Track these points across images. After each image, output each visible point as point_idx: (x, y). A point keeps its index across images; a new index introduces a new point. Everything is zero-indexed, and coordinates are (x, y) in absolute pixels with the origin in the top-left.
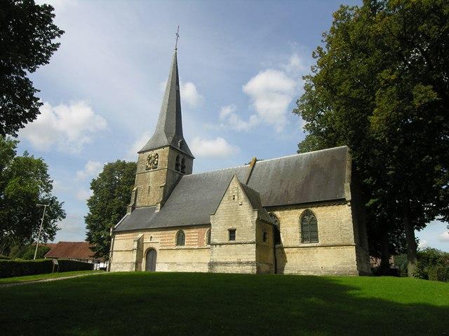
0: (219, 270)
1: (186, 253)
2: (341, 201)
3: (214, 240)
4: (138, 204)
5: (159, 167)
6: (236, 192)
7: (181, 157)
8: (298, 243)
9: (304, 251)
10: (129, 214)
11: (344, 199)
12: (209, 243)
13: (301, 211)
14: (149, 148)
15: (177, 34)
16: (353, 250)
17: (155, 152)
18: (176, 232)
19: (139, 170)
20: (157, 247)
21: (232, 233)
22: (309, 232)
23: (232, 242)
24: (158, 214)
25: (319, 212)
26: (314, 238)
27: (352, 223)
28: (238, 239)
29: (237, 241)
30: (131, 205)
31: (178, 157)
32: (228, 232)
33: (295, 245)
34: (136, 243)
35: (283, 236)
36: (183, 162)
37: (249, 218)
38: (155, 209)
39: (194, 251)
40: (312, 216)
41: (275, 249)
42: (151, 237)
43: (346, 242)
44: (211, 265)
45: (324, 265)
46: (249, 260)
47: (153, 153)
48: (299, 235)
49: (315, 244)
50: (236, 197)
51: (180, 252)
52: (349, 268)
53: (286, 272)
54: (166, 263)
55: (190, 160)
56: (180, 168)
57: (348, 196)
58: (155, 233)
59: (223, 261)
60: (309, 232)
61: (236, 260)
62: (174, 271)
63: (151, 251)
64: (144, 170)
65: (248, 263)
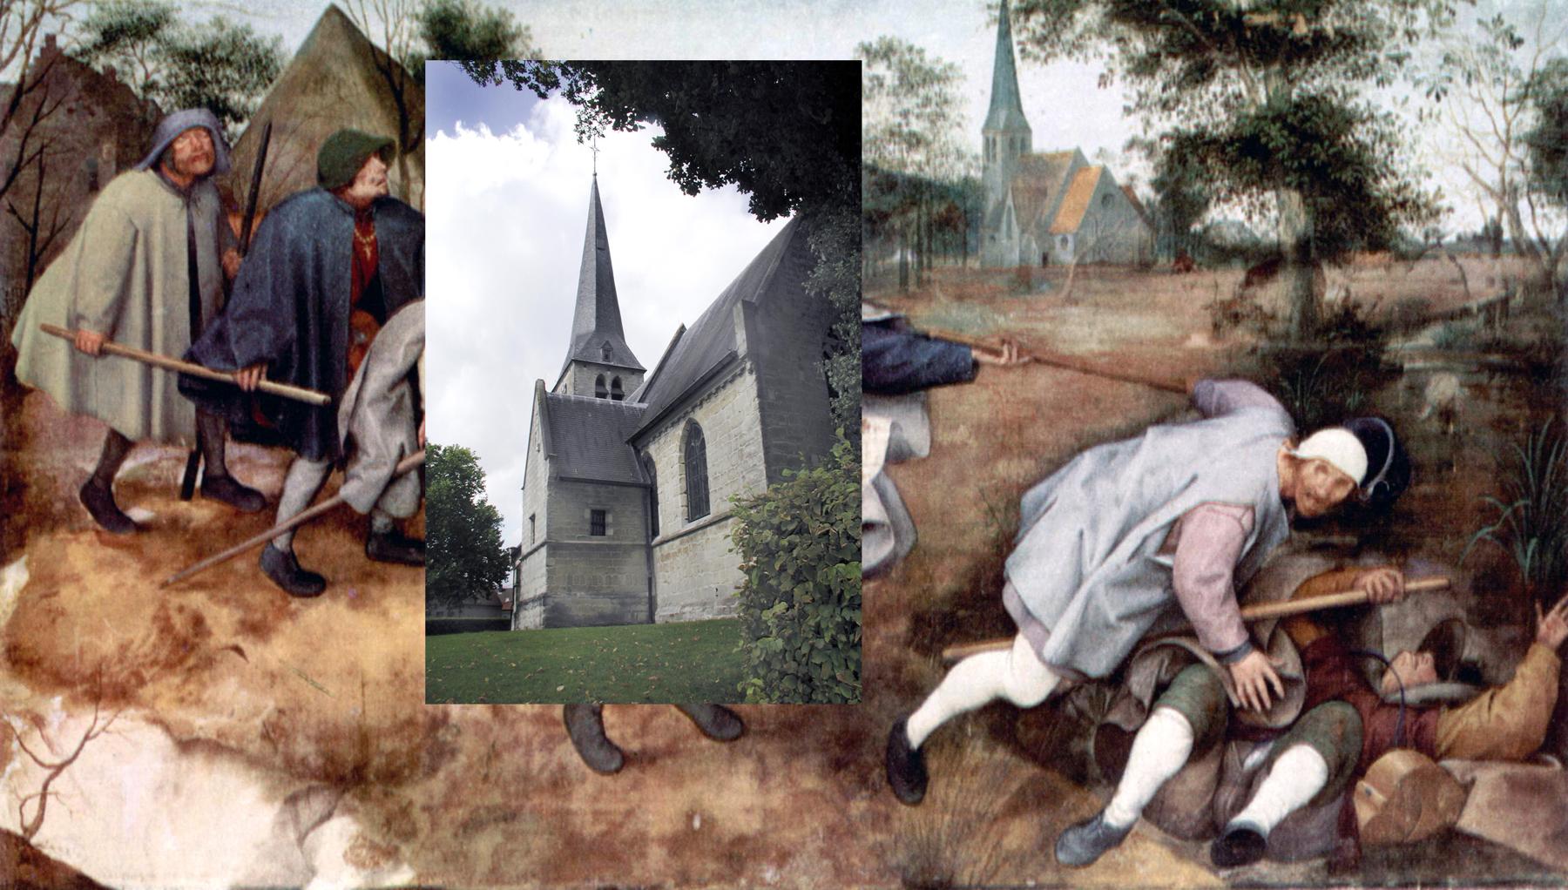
11: (733, 357)
31: (600, 382)
55: (635, 377)
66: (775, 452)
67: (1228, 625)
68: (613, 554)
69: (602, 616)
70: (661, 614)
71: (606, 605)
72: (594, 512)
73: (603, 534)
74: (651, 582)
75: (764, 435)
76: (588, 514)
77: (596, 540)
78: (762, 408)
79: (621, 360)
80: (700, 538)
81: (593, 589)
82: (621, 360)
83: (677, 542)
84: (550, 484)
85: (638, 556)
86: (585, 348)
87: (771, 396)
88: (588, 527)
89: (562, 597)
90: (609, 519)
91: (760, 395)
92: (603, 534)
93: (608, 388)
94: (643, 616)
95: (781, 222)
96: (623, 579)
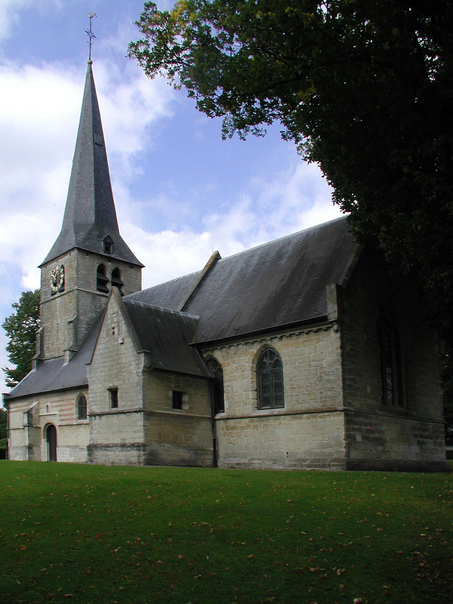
1: (295, 423)
2: (318, 323)
3: (92, 407)
4: (47, 355)
5: (67, 288)
6: (115, 320)
7: (110, 267)
8: (249, 409)
9: (260, 424)
10: (34, 371)
11: (324, 319)
12: (82, 413)
13: (255, 349)
14: (52, 258)
15: (89, 33)
16: (340, 419)
19: (43, 299)
20: (56, 422)
21: (114, 392)
22: (269, 388)
23: (115, 410)
24: (67, 366)
25: (287, 348)
26: (279, 401)
27: (340, 367)
28: (122, 404)
29: (119, 409)
30: (36, 356)
31: (101, 270)
32: (107, 394)
33: (246, 413)
34: (26, 415)
35: (227, 396)
36: (116, 274)
37: (133, 368)
38: (63, 361)
39: (74, 427)
40: (276, 358)
43: (329, 404)
44: (91, 448)
47: (56, 266)
48: (252, 395)
49: (276, 411)
50: (116, 330)
52: (331, 454)
54: (67, 447)
55: (133, 271)
57: (332, 311)
59: (104, 442)
60: (269, 388)
61: (118, 441)
62: (77, 461)
63: (51, 430)
64: (50, 297)
65: (133, 446)
66: (348, 382)
67: (35, 419)
68: (189, 420)
69: (182, 460)
70: (221, 461)
71: (185, 454)
72: (174, 393)
73: (180, 407)
74: (215, 442)
75: (343, 372)
76: (171, 394)
77: (176, 412)
78: (343, 355)
79: (121, 254)
80: (272, 421)
81: (175, 442)
82: (121, 254)
83: (247, 420)
84: (144, 371)
85: (206, 425)
86: (86, 239)
87: (348, 348)
88: (171, 403)
89: (155, 447)
90: (185, 398)
91: (342, 347)
92: (180, 407)
93: (109, 276)
94: (209, 462)
95: (348, 214)
96: (195, 438)
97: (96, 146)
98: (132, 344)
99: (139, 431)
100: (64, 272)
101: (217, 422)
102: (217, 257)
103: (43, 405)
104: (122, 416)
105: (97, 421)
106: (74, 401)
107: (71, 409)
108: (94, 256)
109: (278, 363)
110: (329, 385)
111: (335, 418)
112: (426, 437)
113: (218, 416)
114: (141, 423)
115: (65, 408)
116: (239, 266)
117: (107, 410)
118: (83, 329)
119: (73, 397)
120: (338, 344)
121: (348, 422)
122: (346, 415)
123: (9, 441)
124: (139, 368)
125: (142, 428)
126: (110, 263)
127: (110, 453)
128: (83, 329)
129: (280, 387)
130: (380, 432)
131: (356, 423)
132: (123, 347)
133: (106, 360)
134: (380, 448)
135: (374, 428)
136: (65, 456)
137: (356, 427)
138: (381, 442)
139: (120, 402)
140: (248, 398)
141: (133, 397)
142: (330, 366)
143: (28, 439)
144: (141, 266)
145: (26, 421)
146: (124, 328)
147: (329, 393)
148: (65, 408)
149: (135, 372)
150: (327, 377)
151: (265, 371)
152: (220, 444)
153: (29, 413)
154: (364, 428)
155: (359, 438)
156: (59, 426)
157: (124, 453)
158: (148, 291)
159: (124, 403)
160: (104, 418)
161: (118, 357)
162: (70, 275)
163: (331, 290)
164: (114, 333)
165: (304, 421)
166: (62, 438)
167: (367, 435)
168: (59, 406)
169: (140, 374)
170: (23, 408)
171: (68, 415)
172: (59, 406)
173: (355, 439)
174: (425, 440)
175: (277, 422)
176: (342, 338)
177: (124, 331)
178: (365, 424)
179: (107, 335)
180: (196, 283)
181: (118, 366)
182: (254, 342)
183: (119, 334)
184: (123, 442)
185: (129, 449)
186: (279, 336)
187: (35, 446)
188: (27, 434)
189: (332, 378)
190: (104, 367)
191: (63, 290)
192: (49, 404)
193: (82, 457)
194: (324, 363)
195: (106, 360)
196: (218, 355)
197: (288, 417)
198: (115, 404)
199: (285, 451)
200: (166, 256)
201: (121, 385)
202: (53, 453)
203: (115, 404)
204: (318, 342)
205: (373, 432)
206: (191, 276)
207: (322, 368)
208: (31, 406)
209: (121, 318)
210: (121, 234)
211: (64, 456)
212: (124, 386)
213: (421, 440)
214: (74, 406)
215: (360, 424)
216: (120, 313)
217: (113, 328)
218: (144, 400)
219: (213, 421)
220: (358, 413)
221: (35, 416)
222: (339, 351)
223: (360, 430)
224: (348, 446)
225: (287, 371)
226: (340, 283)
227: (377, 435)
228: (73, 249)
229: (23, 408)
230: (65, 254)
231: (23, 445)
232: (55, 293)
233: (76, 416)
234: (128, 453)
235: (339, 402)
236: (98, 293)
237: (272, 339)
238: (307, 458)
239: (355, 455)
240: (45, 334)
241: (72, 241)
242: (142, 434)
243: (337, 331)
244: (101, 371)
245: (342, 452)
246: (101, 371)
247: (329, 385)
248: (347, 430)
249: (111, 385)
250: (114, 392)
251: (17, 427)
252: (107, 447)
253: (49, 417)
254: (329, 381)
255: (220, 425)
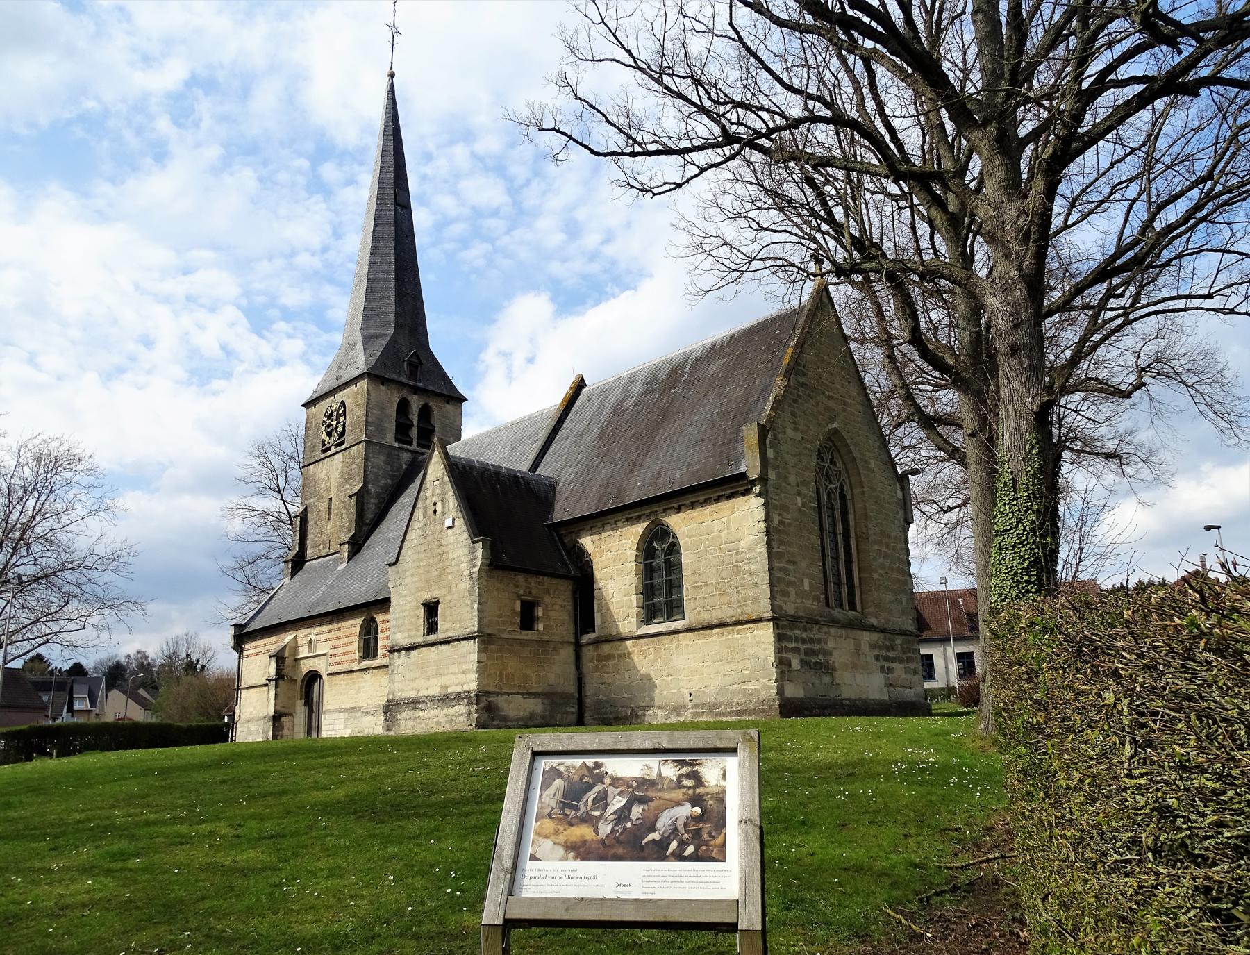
0: (411, 724)
7: (416, 403)
12: (369, 648)
14: (326, 389)
16: (766, 633)
17: (340, 397)
18: (359, 621)
21: (431, 609)
22: (661, 588)
23: (432, 637)
26: (674, 608)
28: (446, 627)
29: (440, 635)
31: (403, 407)
32: (421, 612)
36: (425, 412)
41: (578, 647)
42: (311, 642)
44: (391, 708)
45: (696, 684)
46: (450, 691)
47: (331, 403)
50: (439, 508)
51: (368, 676)
53: (324, 734)
56: (414, 433)
58: (319, 629)
59: (412, 694)
60: (661, 588)
61: (434, 690)
65: (459, 698)
68: (543, 648)
72: (523, 603)
73: (531, 628)
77: (526, 635)
88: (518, 620)
90: (540, 612)
91: (767, 520)
92: (531, 628)
97: (399, 209)
98: (464, 528)
99: (469, 671)
100: (344, 412)
101: (584, 650)
102: (580, 385)
103: (303, 641)
104: (444, 647)
105: (400, 659)
106: (357, 630)
107: (351, 644)
108: (393, 386)
109: (674, 549)
110: (749, 580)
111: (761, 633)
112: (893, 660)
113: (585, 639)
114: (475, 657)
115: (341, 641)
116: (613, 399)
117: (420, 639)
118: (372, 506)
119: (353, 626)
120: (761, 514)
121: (780, 638)
122: (776, 627)
123: (237, 711)
124: (474, 566)
125: (476, 666)
126: (415, 397)
127: (420, 713)
128: (373, 507)
129: (674, 586)
130: (827, 653)
131: (790, 639)
132: (450, 532)
133: (422, 555)
134: (827, 679)
135: (816, 647)
136: (337, 727)
137: (791, 645)
138: (826, 668)
139: (442, 624)
140: (630, 607)
141: (461, 615)
142: (751, 549)
143: (273, 702)
144: (463, 399)
145: (272, 671)
146: (452, 503)
147: (751, 593)
148: (341, 641)
149: (466, 573)
150: (747, 567)
151: (655, 563)
152: (587, 687)
153: (279, 657)
154: (803, 647)
155: (795, 664)
156: (329, 675)
157: (445, 711)
158: (473, 440)
159: (448, 626)
160: (414, 653)
161: (441, 550)
162: (356, 415)
163: (750, 435)
164: (435, 512)
165: (714, 639)
166: (333, 695)
167: (807, 658)
168: (330, 639)
169: (475, 576)
170: (267, 648)
171: (345, 654)
172: (330, 639)
173: (790, 666)
174: (892, 665)
175: (674, 644)
176: (766, 505)
177: (451, 505)
178: (804, 641)
179: (425, 515)
180: (549, 424)
181: (440, 566)
182: (639, 517)
183: (443, 513)
184: (444, 692)
185: (454, 703)
186: (676, 505)
187: (286, 715)
188: (272, 693)
189: (753, 567)
190: (418, 567)
191: (342, 443)
192: (313, 637)
193: (373, 726)
194: (743, 545)
195: (422, 555)
196: (587, 542)
197: (690, 634)
198: (432, 627)
199: (687, 691)
200: (512, 384)
201: (444, 596)
202: (312, 725)
203: (432, 627)
204: (733, 513)
205: (815, 653)
206: (541, 413)
207: (738, 553)
208: (282, 644)
209: (449, 487)
210: (434, 346)
211: (333, 727)
212: (448, 598)
213: (886, 664)
214: (357, 638)
215: (797, 640)
216: (446, 478)
217: (435, 504)
218: (480, 619)
219: (578, 647)
220: (794, 621)
221: (289, 662)
222: (763, 525)
223: (796, 650)
224: (781, 678)
225: (687, 559)
226: (763, 422)
227: (821, 658)
228: (361, 377)
229: (267, 648)
230: (347, 384)
231: (261, 715)
232: (329, 449)
233: (356, 656)
234: (452, 710)
235: (764, 607)
236: (397, 445)
237: (665, 511)
238: (721, 700)
239: (793, 691)
240: (310, 517)
241: (361, 363)
242: (474, 676)
243: (759, 495)
244: (412, 575)
245: (772, 687)
246: (412, 575)
247: (749, 580)
248: (778, 650)
249: (427, 597)
250: (431, 609)
251: (253, 683)
252: (415, 703)
253: (311, 661)
254: (750, 572)
255: (588, 653)
